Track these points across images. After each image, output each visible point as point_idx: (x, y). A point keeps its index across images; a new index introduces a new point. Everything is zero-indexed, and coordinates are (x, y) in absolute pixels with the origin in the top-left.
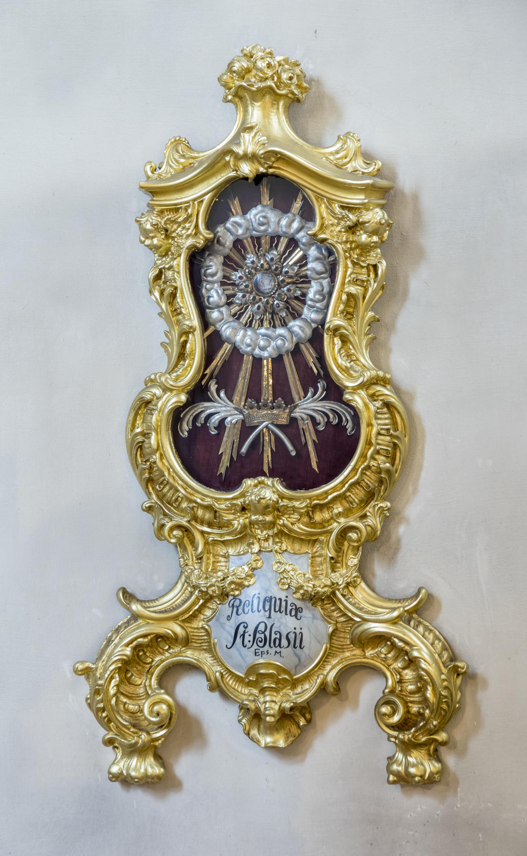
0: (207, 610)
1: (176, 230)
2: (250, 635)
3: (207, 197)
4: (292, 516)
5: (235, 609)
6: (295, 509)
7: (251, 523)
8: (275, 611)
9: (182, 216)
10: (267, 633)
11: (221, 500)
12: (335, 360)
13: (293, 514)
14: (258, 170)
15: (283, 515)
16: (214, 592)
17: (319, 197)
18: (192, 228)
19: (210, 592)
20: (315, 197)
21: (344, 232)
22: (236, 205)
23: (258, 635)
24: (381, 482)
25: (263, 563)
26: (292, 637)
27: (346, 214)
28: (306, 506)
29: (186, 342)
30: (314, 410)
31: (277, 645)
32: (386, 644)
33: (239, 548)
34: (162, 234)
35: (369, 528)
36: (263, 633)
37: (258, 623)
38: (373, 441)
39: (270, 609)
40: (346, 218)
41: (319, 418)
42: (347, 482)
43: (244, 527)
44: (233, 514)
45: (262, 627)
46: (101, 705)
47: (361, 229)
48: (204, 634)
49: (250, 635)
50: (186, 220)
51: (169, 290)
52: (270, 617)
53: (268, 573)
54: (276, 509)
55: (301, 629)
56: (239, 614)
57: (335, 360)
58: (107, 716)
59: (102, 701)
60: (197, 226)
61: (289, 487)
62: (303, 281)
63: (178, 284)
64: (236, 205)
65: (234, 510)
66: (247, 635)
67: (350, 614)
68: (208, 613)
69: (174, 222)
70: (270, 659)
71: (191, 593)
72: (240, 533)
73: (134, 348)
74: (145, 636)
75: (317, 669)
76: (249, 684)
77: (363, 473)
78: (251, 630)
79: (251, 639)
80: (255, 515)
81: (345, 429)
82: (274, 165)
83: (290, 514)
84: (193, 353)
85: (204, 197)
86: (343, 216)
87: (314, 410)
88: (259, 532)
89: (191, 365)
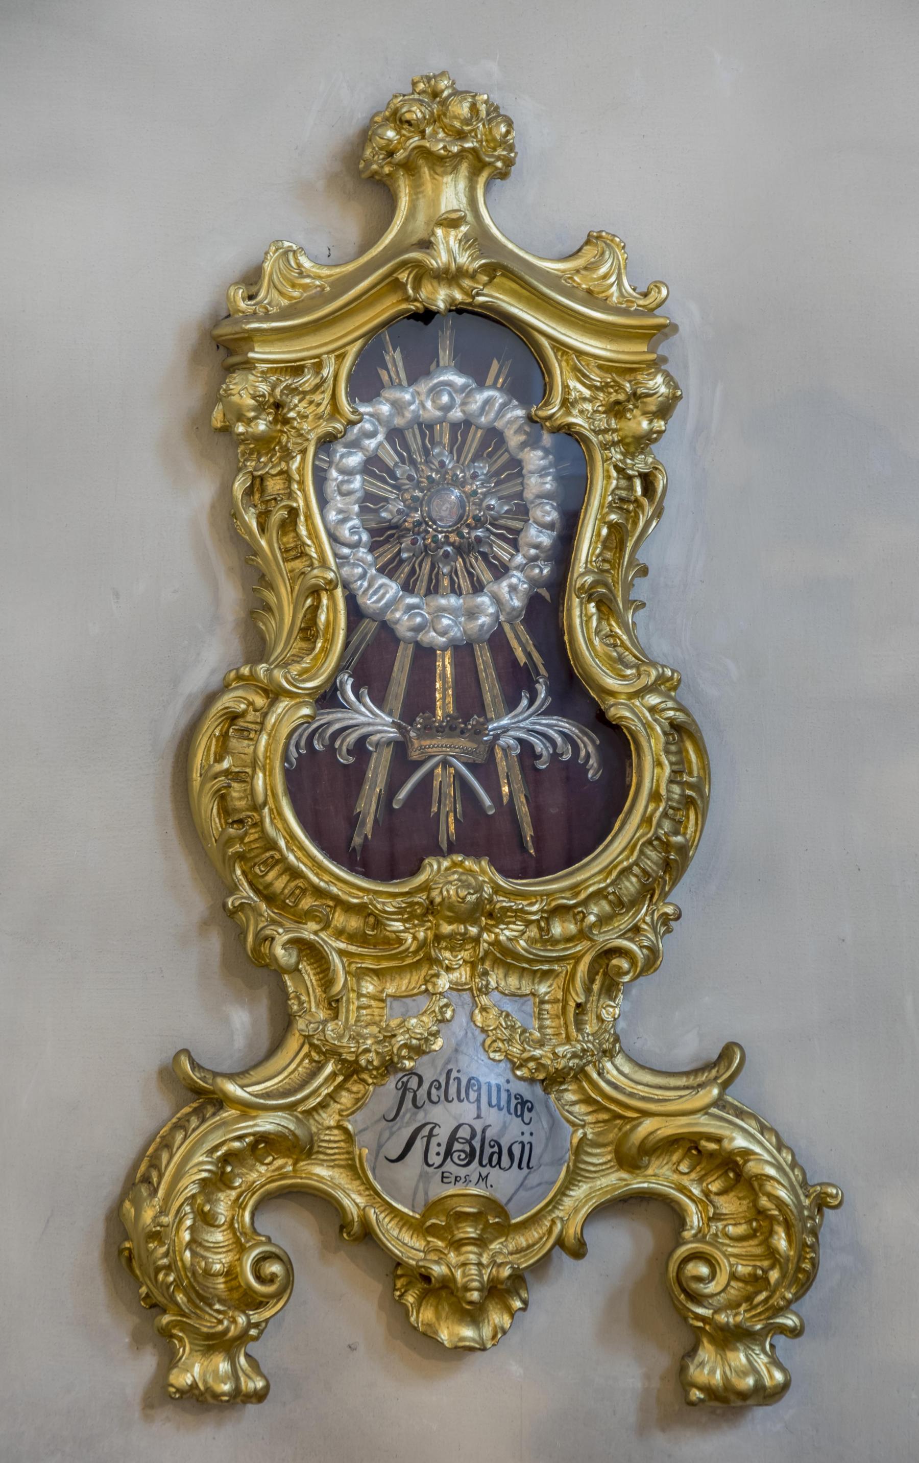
0: (344, 1093)
1: (296, 406)
2: (439, 1145)
3: (353, 350)
4: (511, 926)
5: (409, 1096)
6: (519, 914)
7: (438, 938)
9: (308, 380)
10: (477, 1143)
11: (386, 896)
13: (514, 923)
14: (453, 300)
15: (496, 926)
16: (370, 1062)
17: (558, 349)
18: (325, 402)
19: (363, 1062)
20: (553, 348)
21: (604, 413)
22: (395, 357)
23: (457, 1146)
24: (667, 865)
25: (454, 1010)
27: (614, 381)
28: (542, 911)
30: (529, 731)
31: (494, 1164)
32: (726, 1173)
33: (405, 982)
34: (270, 413)
35: (645, 951)
37: (834, 1183)
38: (663, 792)
39: (478, 1100)
40: (612, 387)
41: (539, 746)
42: (615, 867)
43: (423, 945)
44: (404, 921)
45: (464, 1133)
46: (165, 1261)
47: (636, 407)
48: (337, 1138)
49: (439, 1145)
50: (317, 387)
53: (471, 1031)
54: (484, 912)
55: (531, 1134)
58: (175, 1280)
59: (166, 1254)
61: (507, 873)
64: (395, 357)
65: (409, 913)
66: (434, 1141)
67: (613, 1107)
68: (346, 1099)
70: (469, 1187)
73: (125, 595)
74: (240, 1138)
75: (550, 1207)
76: (433, 1231)
77: (642, 852)
78: (442, 1135)
79: (442, 1150)
80: (450, 923)
82: (485, 291)
83: (510, 923)
85: (347, 348)
86: (607, 383)
87: (529, 731)
88: (447, 954)
89: (326, 651)
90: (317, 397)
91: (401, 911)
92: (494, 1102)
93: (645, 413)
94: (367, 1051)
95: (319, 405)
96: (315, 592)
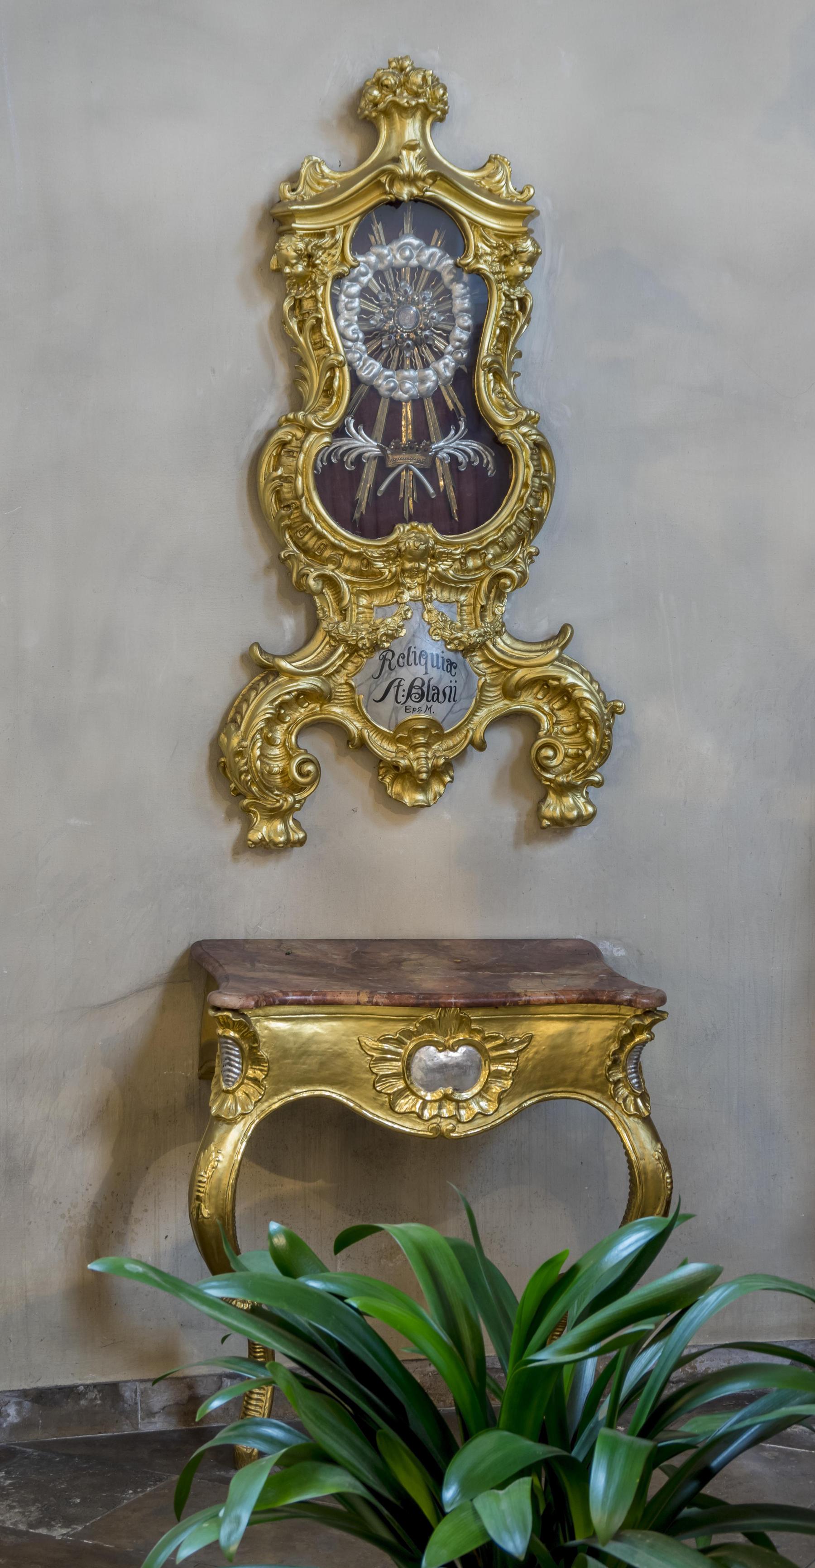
0: (349, 664)
5: (387, 663)
6: (449, 555)
7: (403, 571)
8: (433, 666)
9: (327, 241)
10: (425, 689)
11: (373, 547)
12: (489, 396)
16: (364, 645)
18: (338, 254)
23: (414, 691)
24: (532, 524)
26: (447, 691)
28: (462, 553)
29: (332, 379)
30: (455, 449)
32: (563, 698)
33: (385, 597)
36: (421, 688)
38: (530, 482)
39: (426, 664)
43: (395, 575)
45: (418, 683)
50: (333, 246)
51: (310, 322)
52: (426, 673)
53: (421, 623)
54: (430, 555)
56: (392, 667)
57: (489, 396)
59: (246, 764)
60: (343, 251)
61: (442, 532)
62: (329, 336)
63: (323, 315)
66: (401, 689)
67: (501, 664)
69: (318, 247)
71: (335, 649)
72: (390, 580)
74: (289, 693)
76: (400, 740)
77: (518, 517)
78: (406, 685)
79: (406, 694)
81: (486, 470)
84: (341, 388)
87: (455, 449)
88: (408, 580)
89: (338, 404)
90: (333, 251)
91: (382, 556)
92: (435, 664)
93: (521, 262)
94: (363, 638)
95: (334, 256)
96: (332, 368)
